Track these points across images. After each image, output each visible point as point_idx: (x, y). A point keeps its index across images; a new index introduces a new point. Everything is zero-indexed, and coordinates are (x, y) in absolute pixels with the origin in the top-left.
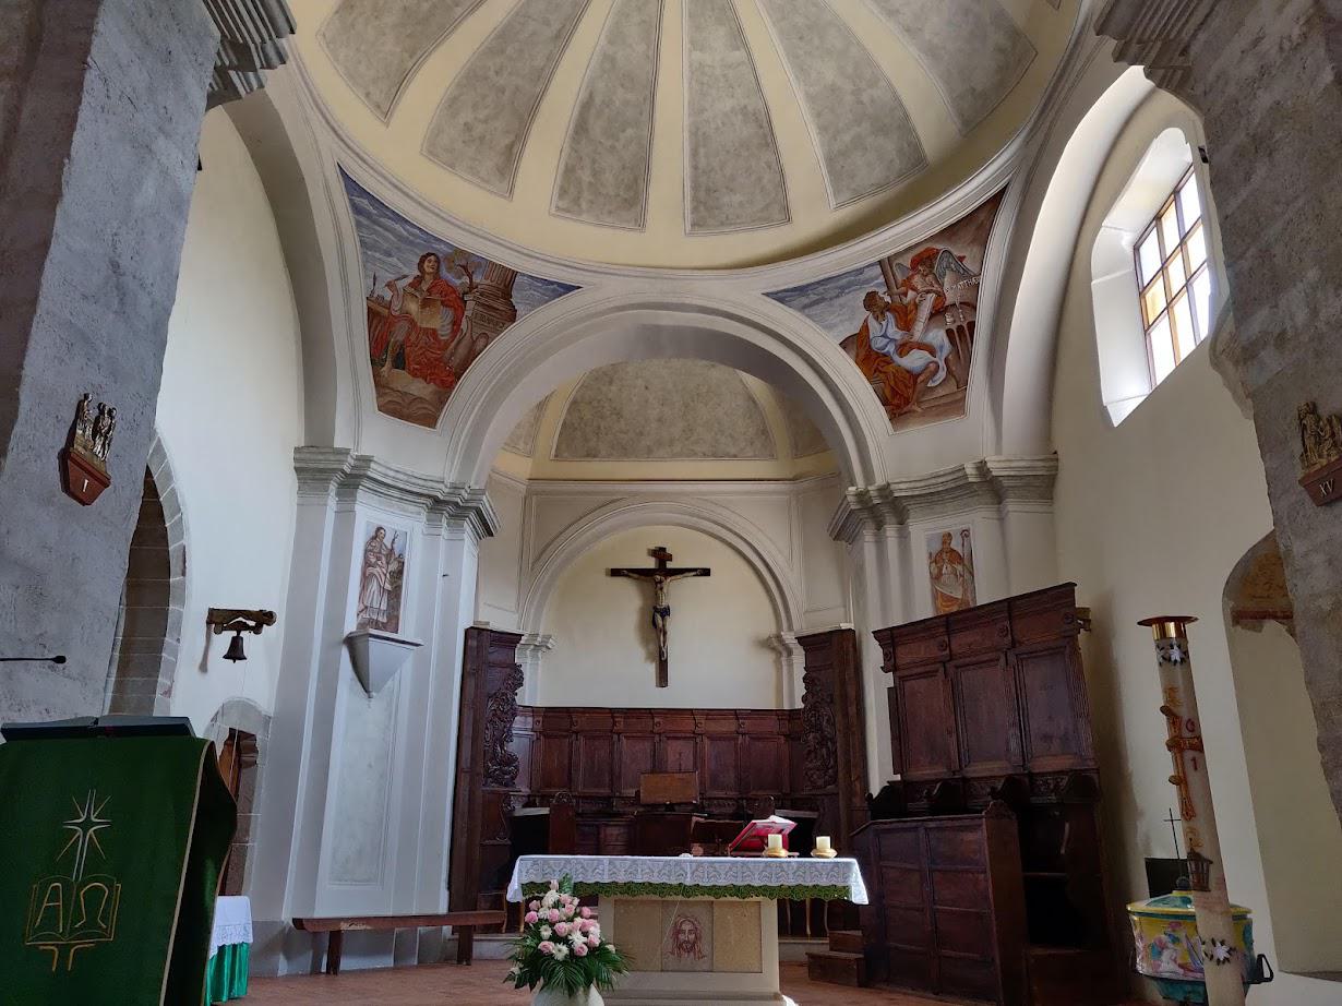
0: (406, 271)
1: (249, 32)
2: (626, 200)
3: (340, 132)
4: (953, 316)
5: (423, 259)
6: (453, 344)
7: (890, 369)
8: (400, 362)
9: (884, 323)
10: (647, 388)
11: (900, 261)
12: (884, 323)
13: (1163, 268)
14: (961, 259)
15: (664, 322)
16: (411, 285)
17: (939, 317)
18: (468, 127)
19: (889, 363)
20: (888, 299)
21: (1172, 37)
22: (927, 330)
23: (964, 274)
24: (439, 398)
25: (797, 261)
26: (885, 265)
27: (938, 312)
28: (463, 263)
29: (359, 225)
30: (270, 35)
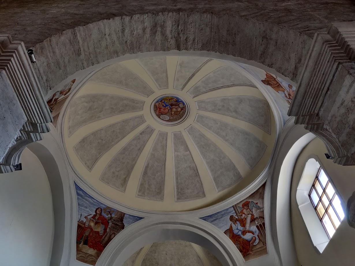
0: (91, 213)
1: (37, 119)
2: (158, 192)
3: (76, 172)
4: (257, 221)
5: (97, 209)
6: (104, 236)
7: (241, 240)
8: (86, 243)
9: (237, 225)
10: (166, 254)
11: (238, 205)
12: (237, 225)
13: (320, 200)
14: (257, 203)
15: (170, 228)
16: (92, 217)
17: (253, 222)
18: (114, 173)
19: (240, 238)
20: (237, 217)
21: (312, 113)
22: (250, 226)
23: (259, 208)
24: (98, 255)
25: (208, 208)
26: (234, 207)
27: (253, 220)
28: (109, 211)
29: (78, 199)
30: (44, 121)
